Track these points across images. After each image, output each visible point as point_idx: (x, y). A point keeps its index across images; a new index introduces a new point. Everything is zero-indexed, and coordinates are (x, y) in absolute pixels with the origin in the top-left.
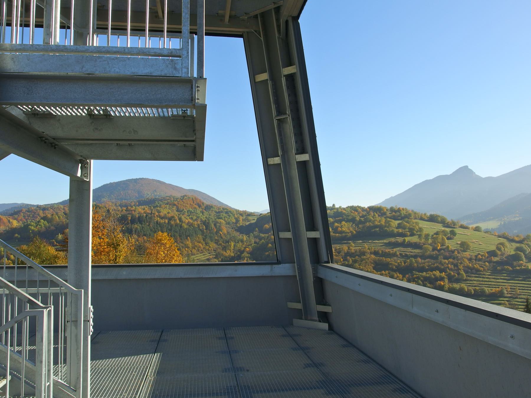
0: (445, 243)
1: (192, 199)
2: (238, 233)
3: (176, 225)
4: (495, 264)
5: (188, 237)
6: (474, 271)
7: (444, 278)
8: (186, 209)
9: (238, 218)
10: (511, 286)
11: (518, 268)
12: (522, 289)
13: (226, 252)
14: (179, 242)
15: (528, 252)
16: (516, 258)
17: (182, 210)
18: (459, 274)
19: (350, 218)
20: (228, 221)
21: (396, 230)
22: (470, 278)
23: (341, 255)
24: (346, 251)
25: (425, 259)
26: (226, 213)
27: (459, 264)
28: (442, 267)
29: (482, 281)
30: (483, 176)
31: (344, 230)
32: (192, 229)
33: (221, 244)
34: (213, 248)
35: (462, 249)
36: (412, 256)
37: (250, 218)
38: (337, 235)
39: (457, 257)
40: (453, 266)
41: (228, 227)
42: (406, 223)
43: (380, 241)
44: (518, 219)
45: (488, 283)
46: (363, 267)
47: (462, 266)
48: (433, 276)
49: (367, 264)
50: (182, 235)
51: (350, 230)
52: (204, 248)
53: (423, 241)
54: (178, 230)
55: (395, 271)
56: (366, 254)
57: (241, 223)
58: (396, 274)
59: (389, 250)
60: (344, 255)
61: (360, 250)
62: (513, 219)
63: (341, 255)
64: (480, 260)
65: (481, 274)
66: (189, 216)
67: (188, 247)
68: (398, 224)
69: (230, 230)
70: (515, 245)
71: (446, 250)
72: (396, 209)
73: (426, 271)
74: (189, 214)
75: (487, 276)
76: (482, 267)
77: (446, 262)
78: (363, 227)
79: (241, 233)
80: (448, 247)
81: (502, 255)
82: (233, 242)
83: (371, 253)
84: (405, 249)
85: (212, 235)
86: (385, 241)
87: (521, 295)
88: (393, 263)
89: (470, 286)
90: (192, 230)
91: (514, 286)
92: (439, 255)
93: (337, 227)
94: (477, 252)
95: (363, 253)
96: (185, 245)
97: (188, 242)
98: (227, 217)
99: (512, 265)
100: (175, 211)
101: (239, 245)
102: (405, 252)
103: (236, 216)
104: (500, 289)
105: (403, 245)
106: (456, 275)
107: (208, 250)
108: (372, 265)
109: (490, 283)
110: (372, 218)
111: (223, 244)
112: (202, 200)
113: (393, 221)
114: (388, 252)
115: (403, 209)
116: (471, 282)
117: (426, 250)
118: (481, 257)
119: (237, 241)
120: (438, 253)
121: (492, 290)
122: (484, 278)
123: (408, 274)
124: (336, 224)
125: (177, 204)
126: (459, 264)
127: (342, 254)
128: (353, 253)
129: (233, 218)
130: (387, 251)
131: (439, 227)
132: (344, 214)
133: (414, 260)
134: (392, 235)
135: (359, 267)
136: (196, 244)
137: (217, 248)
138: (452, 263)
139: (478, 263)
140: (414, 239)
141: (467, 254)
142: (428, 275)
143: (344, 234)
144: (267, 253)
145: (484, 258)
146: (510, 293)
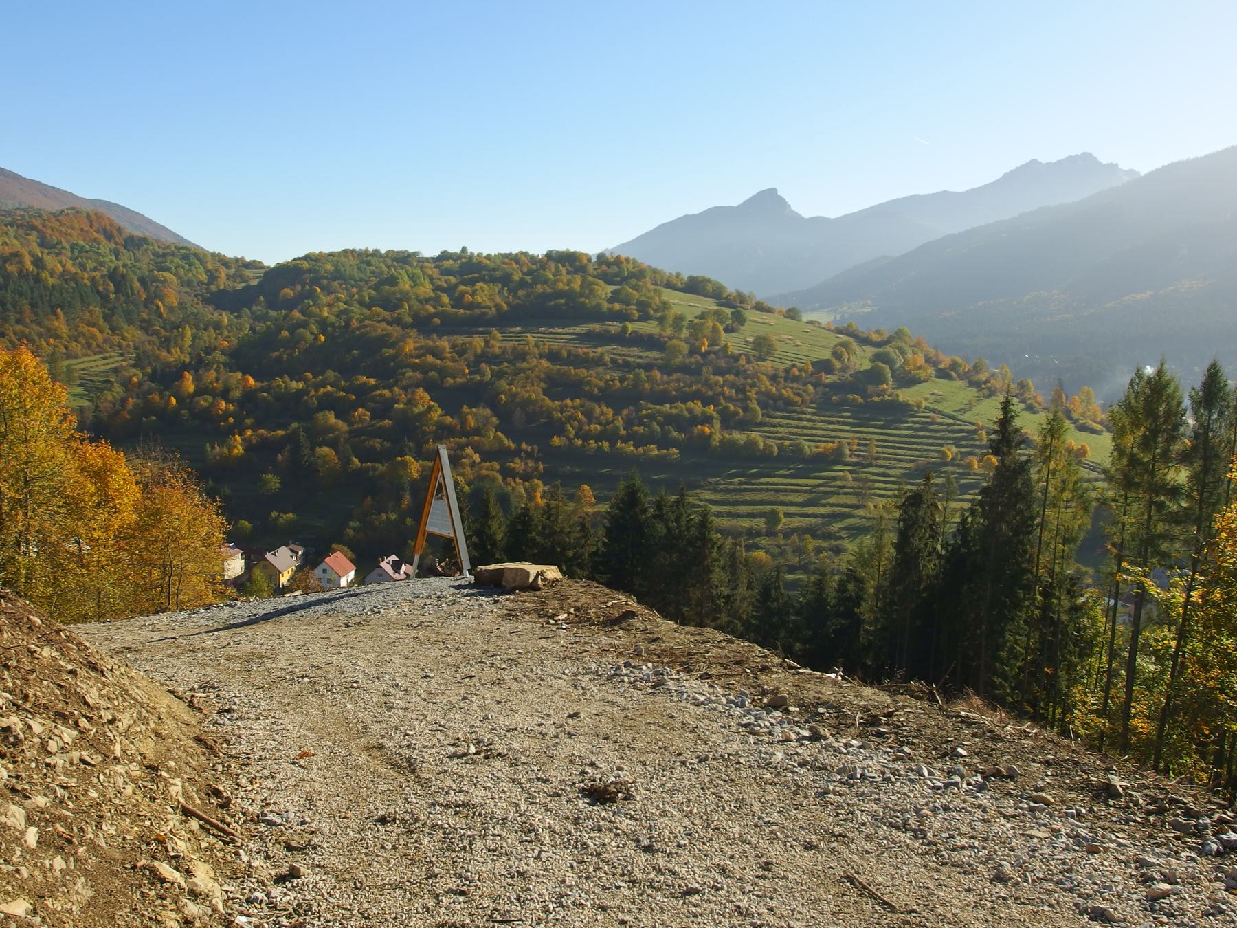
0: (720, 340)
1: (88, 216)
2: (210, 308)
3: (23, 275)
4: (827, 390)
5: (59, 310)
6: (780, 403)
7: (711, 417)
8: (68, 241)
9: (216, 270)
10: (860, 439)
11: (876, 399)
12: (883, 447)
13: (169, 352)
14: (28, 321)
15: (898, 365)
16: (874, 376)
17: (57, 244)
18: (746, 409)
19: (498, 274)
20: (186, 279)
21: (605, 306)
22: (772, 420)
23: (466, 360)
24: (479, 351)
25: (669, 374)
26: (185, 257)
27: (748, 388)
28: (710, 393)
29: (798, 427)
30: (806, 213)
31: (480, 300)
32: (73, 288)
33: (156, 333)
34: (133, 341)
35: (757, 354)
36: (640, 366)
37: (248, 273)
38: (462, 311)
39: (745, 371)
40: (734, 391)
41: (187, 293)
42: (631, 291)
43: (566, 330)
44: (870, 310)
45: (809, 432)
46: (519, 390)
47: (754, 392)
48: (686, 413)
49: (530, 381)
50: (40, 303)
51: (493, 301)
52: (105, 341)
53: (669, 332)
54: (25, 287)
55: (598, 400)
56: (528, 357)
57: (222, 283)
58: (600, 406)
59: (586, 350)
60: (472, 358)
61: (514, 348)
62: (860, 310)
63: (466, 360)
64: (795, 379)
65: (795, 411)
66: (77, 258)
67: (57, 337)
68: (612, 292)
69: (188, 300)
70: (870, 351)
71: (721, 354)
72: (612, 260)
73: (672, 401)
74: (76, 254)
75: (808, 417)
76: (798, 394)
77: (718, 381)
78: (528, 295)
79: (219, 307)
80: (726, 347)
81: (844, 369)
82: (191, 328)
83: (541, 356)
84: (625, 350)
85: (132, 307)
86: (578, 330)
87: (878, 458)
88: (595, 380)
89: (769, 437)
90: (70, 290)
91: (866, 439)
92: (704, 365)
93: (463, 294)
94: (790, 363)
95: (522, 356)
96: (49, 329)
97: (56, 323)
98: (183, 268)
99: (865, 395)
100: (35, 244)
101: (209, 336)
102: (624, 355)
103: (210, 267)
104: (835, 446)
105: (621, 339)
106: (741, 411)
107: (120, 346)
108: (543, 385)
109: (814, 432)
110: (551, 277)
111: (163, 332)
112: (113, 217)
113: (601, 283)
114: (584, 353)
115: (627, 260)
116: (773, 429)
117: (675, 351)
118: (797, 373)
119: (200, 325)
120: (701, 361)
121: (817, 447)
122: (801, 419)
123: (627, 408)
124: (462, 288)
125: (40, 227)
126: (748, 388)
127: (470, 356)
128: (497, 357)
129: (202, 270)
130: (580, 351)
131: (709, 305)
132: (485, 267)
133: (643, 375)
134: (598, 316)
135: (507, 387)
136: (83, 328)
137: (143, 343)
138: (732, 385)
139: (790, 385)
140: (650, 328)
141: (768, 365)
142: (674, 411)
143: (477, 311)
144: (276, 354)
145: (804, 375)
146: (855, 455)
